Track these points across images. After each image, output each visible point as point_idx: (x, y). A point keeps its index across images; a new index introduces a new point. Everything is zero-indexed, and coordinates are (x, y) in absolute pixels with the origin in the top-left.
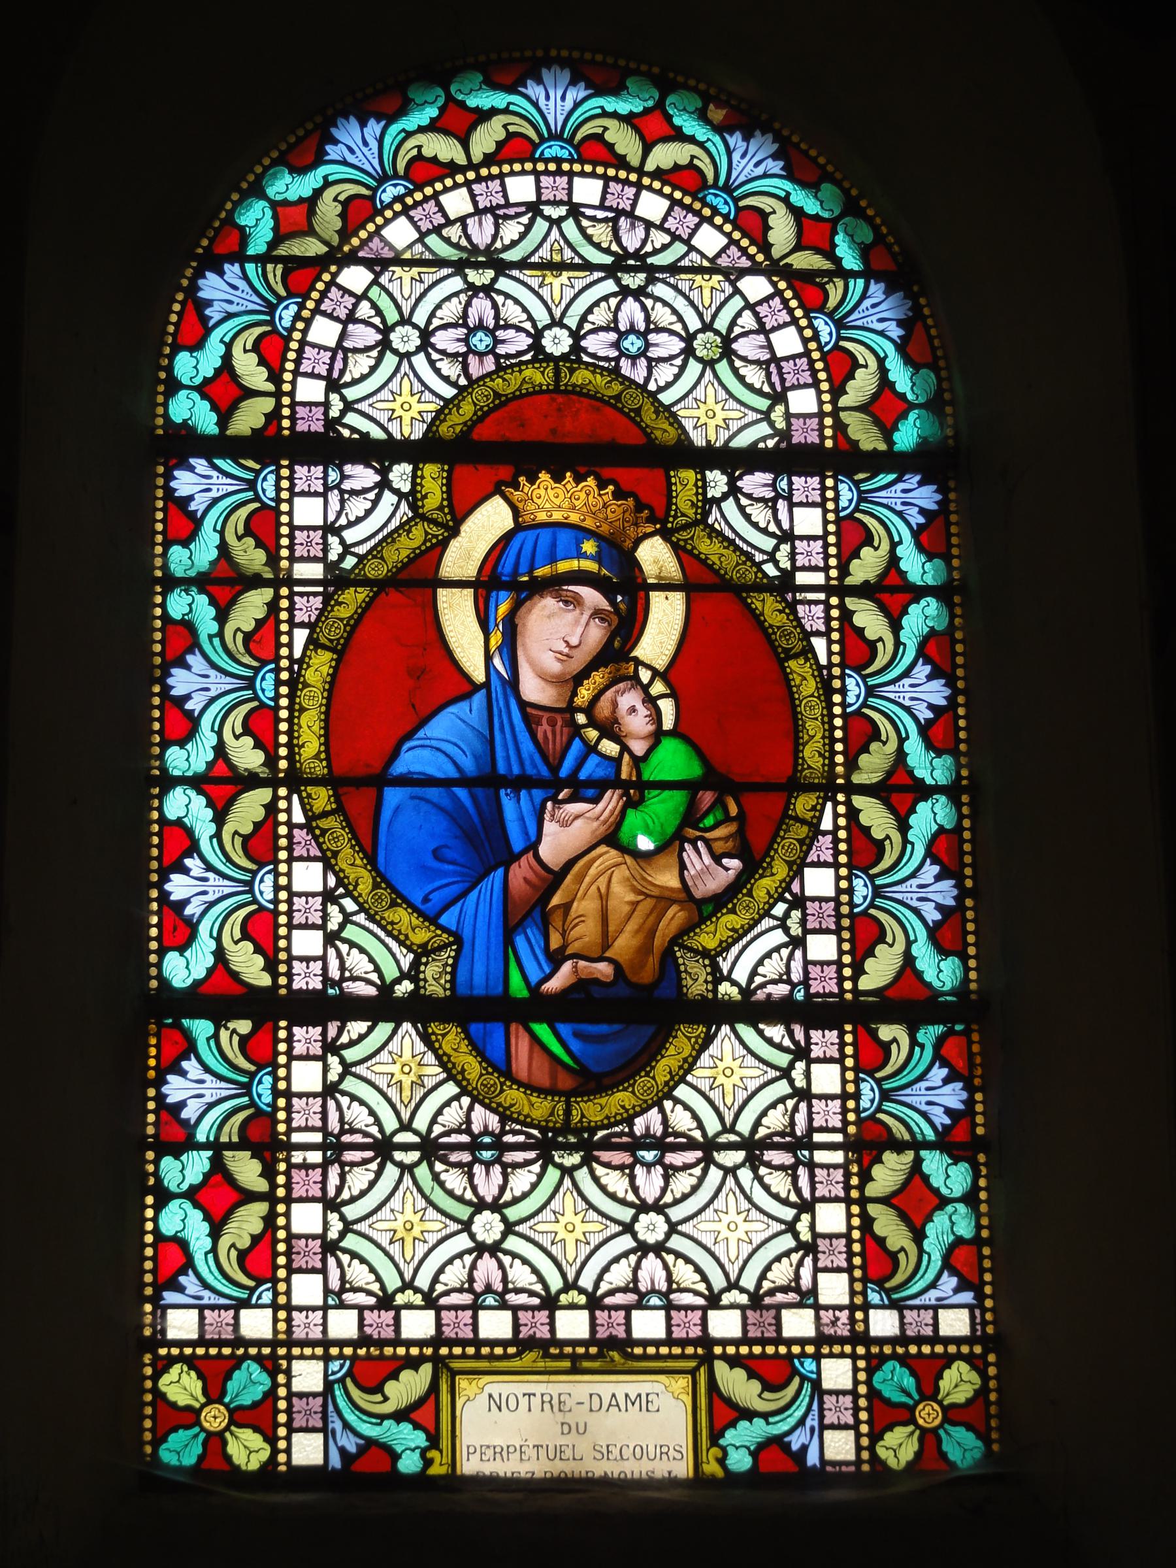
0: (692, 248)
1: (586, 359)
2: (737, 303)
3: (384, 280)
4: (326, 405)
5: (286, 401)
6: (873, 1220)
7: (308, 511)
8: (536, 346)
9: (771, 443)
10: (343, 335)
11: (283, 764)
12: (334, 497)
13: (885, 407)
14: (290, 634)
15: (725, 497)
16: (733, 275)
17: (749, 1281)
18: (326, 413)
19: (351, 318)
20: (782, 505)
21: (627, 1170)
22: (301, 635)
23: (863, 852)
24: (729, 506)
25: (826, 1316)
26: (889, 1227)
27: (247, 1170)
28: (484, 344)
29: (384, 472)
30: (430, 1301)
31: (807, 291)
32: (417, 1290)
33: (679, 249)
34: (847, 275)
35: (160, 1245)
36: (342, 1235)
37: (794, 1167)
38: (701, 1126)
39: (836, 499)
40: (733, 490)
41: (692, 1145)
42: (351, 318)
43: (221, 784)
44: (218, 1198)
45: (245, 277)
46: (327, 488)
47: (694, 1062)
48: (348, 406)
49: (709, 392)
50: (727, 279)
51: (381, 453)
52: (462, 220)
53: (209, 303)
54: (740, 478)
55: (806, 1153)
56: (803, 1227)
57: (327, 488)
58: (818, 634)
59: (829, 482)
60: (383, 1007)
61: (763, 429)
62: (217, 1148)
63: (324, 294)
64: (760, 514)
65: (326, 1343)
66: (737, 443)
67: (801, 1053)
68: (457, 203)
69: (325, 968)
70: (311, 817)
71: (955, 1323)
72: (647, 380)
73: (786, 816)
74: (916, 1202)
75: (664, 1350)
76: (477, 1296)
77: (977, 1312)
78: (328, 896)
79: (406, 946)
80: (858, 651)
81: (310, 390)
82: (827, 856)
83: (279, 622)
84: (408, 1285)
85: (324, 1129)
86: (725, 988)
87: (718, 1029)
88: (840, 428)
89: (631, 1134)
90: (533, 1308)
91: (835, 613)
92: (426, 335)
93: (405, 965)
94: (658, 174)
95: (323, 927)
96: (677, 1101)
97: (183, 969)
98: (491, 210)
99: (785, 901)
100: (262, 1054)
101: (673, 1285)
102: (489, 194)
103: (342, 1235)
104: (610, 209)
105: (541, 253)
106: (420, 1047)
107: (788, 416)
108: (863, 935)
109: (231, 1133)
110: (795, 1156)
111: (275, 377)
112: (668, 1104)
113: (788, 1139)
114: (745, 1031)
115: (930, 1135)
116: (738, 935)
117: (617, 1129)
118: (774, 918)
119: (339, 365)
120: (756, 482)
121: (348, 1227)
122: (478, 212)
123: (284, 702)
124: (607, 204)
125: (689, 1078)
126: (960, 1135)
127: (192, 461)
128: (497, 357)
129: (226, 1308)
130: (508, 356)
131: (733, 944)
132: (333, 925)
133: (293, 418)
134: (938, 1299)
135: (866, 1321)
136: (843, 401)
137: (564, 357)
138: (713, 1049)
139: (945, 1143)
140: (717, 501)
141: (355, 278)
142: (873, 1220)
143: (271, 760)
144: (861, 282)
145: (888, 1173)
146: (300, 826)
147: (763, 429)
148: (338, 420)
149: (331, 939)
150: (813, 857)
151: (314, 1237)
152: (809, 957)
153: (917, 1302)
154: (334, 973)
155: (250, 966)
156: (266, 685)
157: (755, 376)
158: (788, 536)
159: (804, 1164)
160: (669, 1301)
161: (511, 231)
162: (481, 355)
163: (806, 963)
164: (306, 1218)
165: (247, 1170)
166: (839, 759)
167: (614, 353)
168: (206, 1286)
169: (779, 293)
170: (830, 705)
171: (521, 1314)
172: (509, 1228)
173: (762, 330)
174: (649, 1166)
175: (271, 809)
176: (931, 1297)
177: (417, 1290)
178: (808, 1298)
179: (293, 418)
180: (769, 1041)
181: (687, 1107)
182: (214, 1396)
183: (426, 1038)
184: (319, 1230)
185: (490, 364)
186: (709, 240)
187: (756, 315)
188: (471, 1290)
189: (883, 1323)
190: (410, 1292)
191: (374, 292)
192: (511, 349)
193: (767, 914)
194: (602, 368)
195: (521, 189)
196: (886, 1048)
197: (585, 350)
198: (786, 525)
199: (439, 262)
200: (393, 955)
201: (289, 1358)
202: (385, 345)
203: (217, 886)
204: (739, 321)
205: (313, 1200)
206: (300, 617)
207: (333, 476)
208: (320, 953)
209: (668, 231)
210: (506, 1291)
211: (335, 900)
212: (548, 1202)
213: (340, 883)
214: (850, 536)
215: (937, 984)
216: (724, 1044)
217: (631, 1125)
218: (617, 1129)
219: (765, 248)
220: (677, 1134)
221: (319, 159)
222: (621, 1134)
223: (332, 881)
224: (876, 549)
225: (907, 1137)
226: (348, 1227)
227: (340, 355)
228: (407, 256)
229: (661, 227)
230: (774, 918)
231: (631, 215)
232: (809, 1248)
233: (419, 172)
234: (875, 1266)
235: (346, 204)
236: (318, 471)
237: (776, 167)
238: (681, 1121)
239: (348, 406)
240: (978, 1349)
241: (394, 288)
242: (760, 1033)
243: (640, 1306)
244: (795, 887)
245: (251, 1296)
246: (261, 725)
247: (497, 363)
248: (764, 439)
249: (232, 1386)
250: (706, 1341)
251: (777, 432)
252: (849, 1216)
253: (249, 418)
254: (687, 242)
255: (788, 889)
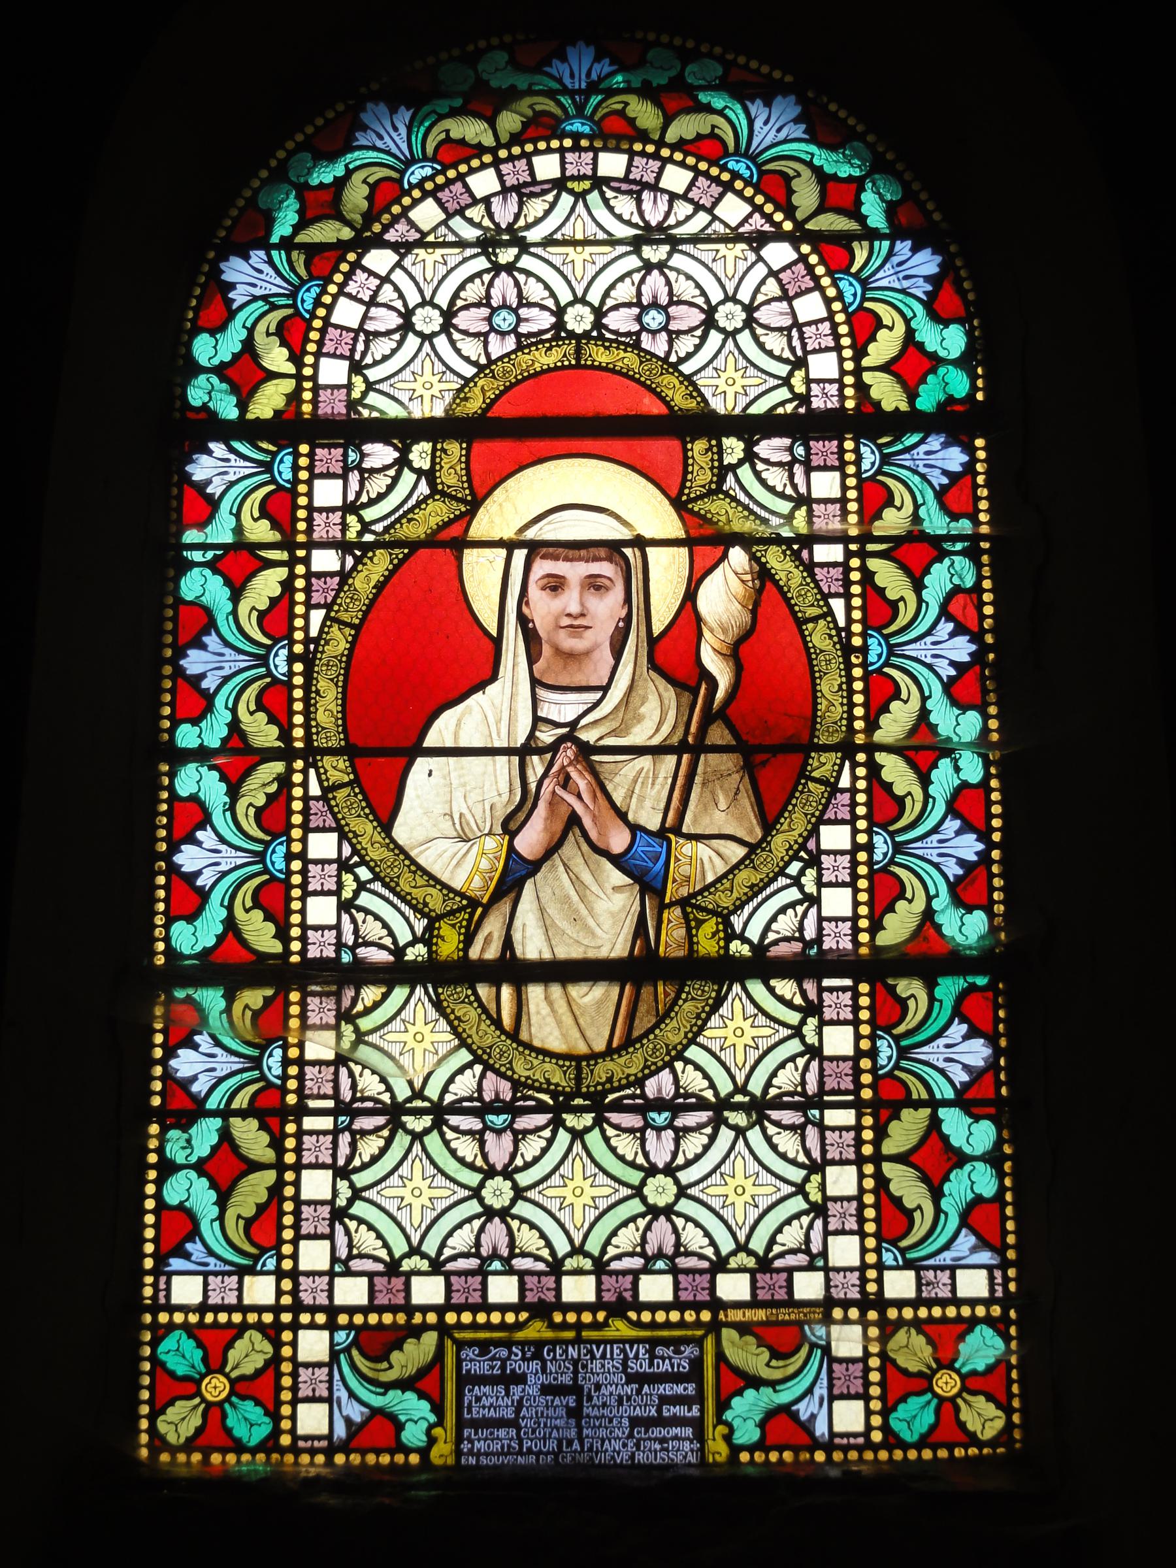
0: (715, 218)
1: (608, 335)
2: (760, 271)
3: (407, 262)
4: (349, 386)
5: (308, 385)
6: (888, 1181)
7: (328, 493)
8: (559, 325)
9: (789, 408)
10: (365, 317)
11: (298, 733)
12: (354, 477)
13: (913, 363)
14: (306, 617)
15: (741, 462)
16: (758, 241)
17: (758, 1244)
18: (349, 394)
19: (372, 302)
20: (798, 470)
21: (639, 1134)
22: (317, 616)
23: (885, 807)
24: (745, 472)
25: (837, 1278)
26: (905, 1184)
27: (252, 1138)
28: (501, 323)
29: (405, 452)
30: (436, 1267)
31: (835, 250)
32: (424, 1256)
33: (703, 218)
34: (871, 235)
35: (164, 1213)
36: (351, 1202)
37: (803, 1127)
38: (712, 1086)
39: (858, 462)
40: (750, 457)
41: (702, 1104)
42: (372, 302)
43: (236, 758)
44: (225, 1168)
45: (270, 262)
46: (347, 470)
47: (705, 1021)
48: (370, 386)
49: (729, 362)
50: (752, 249)
51: (403, 432)
52: (487, 201)
53: (232, 286)
54: (757, 443)
55: (816, 1113)
56: (812, 1188)
57: (347, 470)
58: (837, 595)
59: (849, 445)
60: (398, 973)
61: (783, 394)
62: (225, 1113)
63: (348, 276)
64: (776, 477)
65: (332, 1311)
66: (754, 410)
67: (812, 1009)
68: (484, 182)
69: (339, 936)
70: (328, 791)
71: (973, 1284)
72: (668, 354)
73: (803, 774)
74: (936, 1159)
75: (675, 1316)
76: (484, 1260)
77: (998, 1274)
78: (344, 866)
79: (730, 496)
80: (879, 610)
81: (333, 371)
82: (844, 814)
83: (293, 603)
84: (414, 1251)
85: (336, 1096)
86: (736, 946)
87: (730, 989)
88: (862, 389)
89: (643, 1095)
90: (539, 1274)
91: (855, 576)
92: (448, 315)
93: (419, 930)
94: (681, 145)
95: (337, 893)
96: (687, 1061)
97: (193, 937)
98: (517, 189)
99: (801, 859)
100: (269, 1029)
101: (680, 1249)
102: (515, 173)
103: (351, 1202)
104: (634, 182)
105: (563, 230)
106: (433, 1014)
107: (808, 381)
108: (884, 891)
109: (242, 1101)
110: (805, 1115)
111: (296, 358)
112: (679, 1065)
113: (797, 1098)
114: (757, 988)
115: (950, 1094)
116: (755, 890)
117: (628, 1092)
118: (788, 876)
119: (360, 347)
120: (771, 448)
121: (357, 1194)
122: (505, 191)
123: (298, 680)
124: (631, 177)
125: (700, 1039)
126: (985, 1091)
127: (212, 445)
128: (519, 336)
129: (230, 1274)
130: (530, 335)
131: (747, 902)
132: (347, 894)
133: (315, 402)
134: (954, 1259)
135: (880, 1281)
136: (866, 362)
137: (586, 335)
138: (724, 1010)
139: (965, 1101)
140: (733, 468)
141: (379, 260)
142: (888, 1181)
143: (285, 735)
144: (886, 244)
145: (906, 1131)
146: (317, 799)
147: (783, 394)
148: (360, 401)
149: (345, 906)
150: (830, 815)
151: (323, 1203)
152: (824, 914)
153: (931, 1262)
154: (349, 939)
155: (261, 934)
156: (279, 663)
157: (775, 343)
158: (804, 501)
159: (814, 1124)
160: (674, 1265)
161: (536, 207)
162: (503, 334)
163: (821, 919)
164: (316, 1185)
165: (252, 1138)
166: (859, 712)
167: (636, 327)
168: (211, 1253)
169: (803, 258)
170: (849, 666)
171: (527, 1278)
172: (519, 1193)
173: (786, 297)
174: (659, 1130)
175: (284, 781)
176: (947, 1257)
177: (424, 1256)
178: (817, 1261)
179: (315, 402)
180: (781, 999)
181: (698, 1067)
182: (237, 1387)
183: (438, 1005)
184: (328, 1196)
185: (511, 343)
186: (733, 209)
187: (779, 281)
188: (477, 1255)
189: (900, 1285)
190: (417, 1258)
191: (398, 276)
192: (534, 328)
193: (782, 872)
194: (623, 343)
195: (547, 167)
196: (903, 1003)
197: (606, 327)
198: (803, 489)
199: (462, 244)
200: (407, 919)
201: (295, 1326)
202: (407, 326)
203: (229, 859)
204: (763, 289)
205: (323, 1166)
206: (317, 598)
207: (353, 456)
208: (333, 921)
209: (691, 201)
210: (512, 1255)
211: (350, 869)
212: (557, 1168)
213: (355, 851)
214: (874, 497)
215: (959, 939)
216: (735, 1004)
217: (642, 1087)
218: (628, 1092)
219: (790, 211)
220: (687, 1095)
221: (349, 147)
222: (633, 1097)
223: (347, 850)
224: (899, 509)
225: (924, 1095)
226: (357, 1194)
227: (362, 337)
228: (431, 238)
229: (684, 197)
230: (788, 876)
231: (655, 187)
232: (819, 1210)
233: (447, 155)
234: (891, 1222)
235: (373, 187)
236: (338, 453)
237: (799, 131)
238: (693, 1081)
239: (370, 386)
240: (996, 1311)
241: (416, 271)
242: (771, 990)
243: (646, 1270)
244: (811, 845)
245: (256, 1263)
246: (275, 700)
247: (519, 342)
248: (782, 404)
249: (233, 1355)
250: (716, 1305)
251: (796, 396)
252: (861, 1176)
253: (268, 402)
254: (710, 211)
255: (803, 847)
